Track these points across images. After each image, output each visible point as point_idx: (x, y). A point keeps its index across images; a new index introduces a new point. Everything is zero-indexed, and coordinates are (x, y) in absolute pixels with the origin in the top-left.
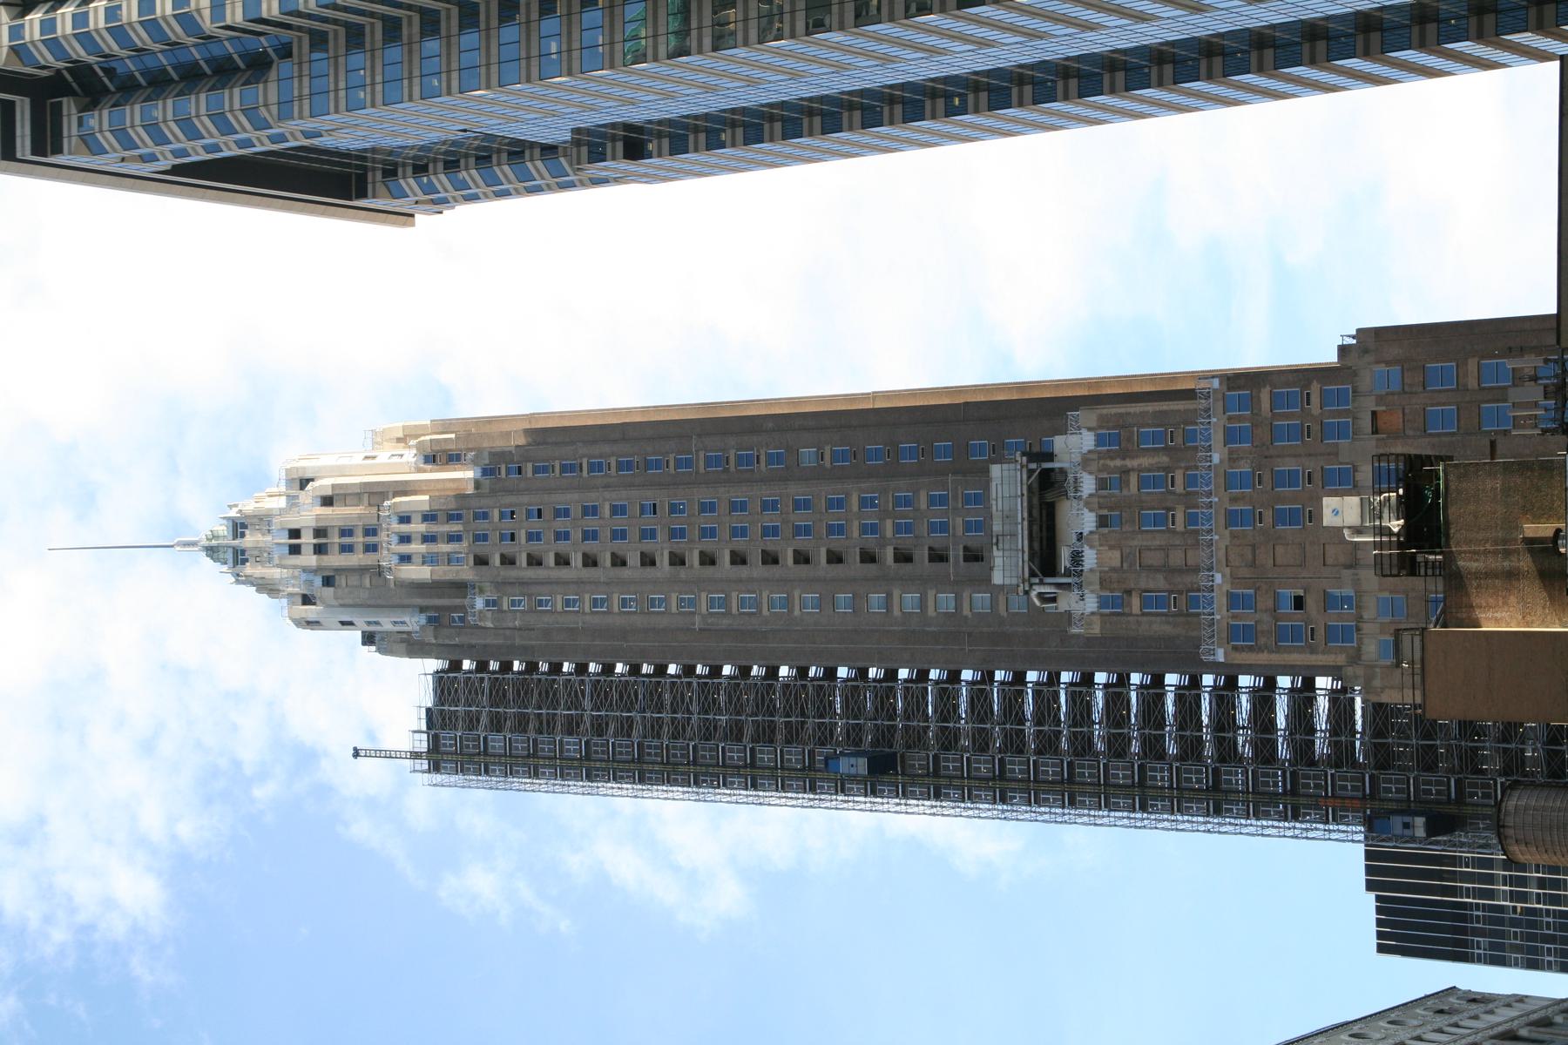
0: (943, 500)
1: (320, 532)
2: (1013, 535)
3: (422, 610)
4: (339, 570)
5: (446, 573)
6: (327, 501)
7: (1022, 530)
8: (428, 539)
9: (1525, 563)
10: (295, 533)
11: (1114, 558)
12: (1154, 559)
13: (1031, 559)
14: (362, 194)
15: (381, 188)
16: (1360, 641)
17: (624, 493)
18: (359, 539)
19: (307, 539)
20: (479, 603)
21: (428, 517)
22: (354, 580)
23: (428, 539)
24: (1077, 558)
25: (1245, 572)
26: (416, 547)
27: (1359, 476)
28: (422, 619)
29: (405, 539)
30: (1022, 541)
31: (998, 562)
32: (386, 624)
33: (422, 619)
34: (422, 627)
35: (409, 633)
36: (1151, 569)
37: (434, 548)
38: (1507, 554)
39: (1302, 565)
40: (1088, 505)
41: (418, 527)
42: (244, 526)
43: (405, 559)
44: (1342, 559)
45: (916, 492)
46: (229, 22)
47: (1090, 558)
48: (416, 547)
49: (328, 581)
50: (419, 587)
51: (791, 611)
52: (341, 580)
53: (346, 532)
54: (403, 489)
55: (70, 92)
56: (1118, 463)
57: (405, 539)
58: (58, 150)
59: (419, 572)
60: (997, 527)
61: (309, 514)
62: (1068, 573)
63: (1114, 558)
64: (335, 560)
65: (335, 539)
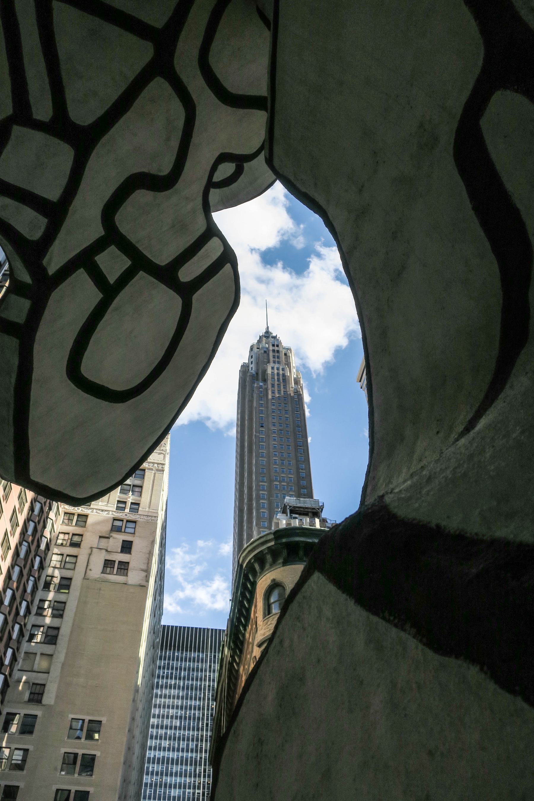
1: (278, 351)
3: (257, 374)
4: (268, 355)
5: (270, 377)
6: (285, 354)
8: (278, 374)
10: (278, 346)
19: (276, 348)
20: (261, 384)
21: (284, 375)
22: (265, 357)
23: (278, 374)
28: (254, 373)
29: (278, 369)
30: (299, 505)
33: (254, 373)
41: (281, 372)
43: (273, 368)
48: (276, 371)
49: (265, 352)
50: (265, 371)
52: (265, 355)
53: (278, 357)
57: (278, 369)
59: (269, 371)
64: (271, 354)
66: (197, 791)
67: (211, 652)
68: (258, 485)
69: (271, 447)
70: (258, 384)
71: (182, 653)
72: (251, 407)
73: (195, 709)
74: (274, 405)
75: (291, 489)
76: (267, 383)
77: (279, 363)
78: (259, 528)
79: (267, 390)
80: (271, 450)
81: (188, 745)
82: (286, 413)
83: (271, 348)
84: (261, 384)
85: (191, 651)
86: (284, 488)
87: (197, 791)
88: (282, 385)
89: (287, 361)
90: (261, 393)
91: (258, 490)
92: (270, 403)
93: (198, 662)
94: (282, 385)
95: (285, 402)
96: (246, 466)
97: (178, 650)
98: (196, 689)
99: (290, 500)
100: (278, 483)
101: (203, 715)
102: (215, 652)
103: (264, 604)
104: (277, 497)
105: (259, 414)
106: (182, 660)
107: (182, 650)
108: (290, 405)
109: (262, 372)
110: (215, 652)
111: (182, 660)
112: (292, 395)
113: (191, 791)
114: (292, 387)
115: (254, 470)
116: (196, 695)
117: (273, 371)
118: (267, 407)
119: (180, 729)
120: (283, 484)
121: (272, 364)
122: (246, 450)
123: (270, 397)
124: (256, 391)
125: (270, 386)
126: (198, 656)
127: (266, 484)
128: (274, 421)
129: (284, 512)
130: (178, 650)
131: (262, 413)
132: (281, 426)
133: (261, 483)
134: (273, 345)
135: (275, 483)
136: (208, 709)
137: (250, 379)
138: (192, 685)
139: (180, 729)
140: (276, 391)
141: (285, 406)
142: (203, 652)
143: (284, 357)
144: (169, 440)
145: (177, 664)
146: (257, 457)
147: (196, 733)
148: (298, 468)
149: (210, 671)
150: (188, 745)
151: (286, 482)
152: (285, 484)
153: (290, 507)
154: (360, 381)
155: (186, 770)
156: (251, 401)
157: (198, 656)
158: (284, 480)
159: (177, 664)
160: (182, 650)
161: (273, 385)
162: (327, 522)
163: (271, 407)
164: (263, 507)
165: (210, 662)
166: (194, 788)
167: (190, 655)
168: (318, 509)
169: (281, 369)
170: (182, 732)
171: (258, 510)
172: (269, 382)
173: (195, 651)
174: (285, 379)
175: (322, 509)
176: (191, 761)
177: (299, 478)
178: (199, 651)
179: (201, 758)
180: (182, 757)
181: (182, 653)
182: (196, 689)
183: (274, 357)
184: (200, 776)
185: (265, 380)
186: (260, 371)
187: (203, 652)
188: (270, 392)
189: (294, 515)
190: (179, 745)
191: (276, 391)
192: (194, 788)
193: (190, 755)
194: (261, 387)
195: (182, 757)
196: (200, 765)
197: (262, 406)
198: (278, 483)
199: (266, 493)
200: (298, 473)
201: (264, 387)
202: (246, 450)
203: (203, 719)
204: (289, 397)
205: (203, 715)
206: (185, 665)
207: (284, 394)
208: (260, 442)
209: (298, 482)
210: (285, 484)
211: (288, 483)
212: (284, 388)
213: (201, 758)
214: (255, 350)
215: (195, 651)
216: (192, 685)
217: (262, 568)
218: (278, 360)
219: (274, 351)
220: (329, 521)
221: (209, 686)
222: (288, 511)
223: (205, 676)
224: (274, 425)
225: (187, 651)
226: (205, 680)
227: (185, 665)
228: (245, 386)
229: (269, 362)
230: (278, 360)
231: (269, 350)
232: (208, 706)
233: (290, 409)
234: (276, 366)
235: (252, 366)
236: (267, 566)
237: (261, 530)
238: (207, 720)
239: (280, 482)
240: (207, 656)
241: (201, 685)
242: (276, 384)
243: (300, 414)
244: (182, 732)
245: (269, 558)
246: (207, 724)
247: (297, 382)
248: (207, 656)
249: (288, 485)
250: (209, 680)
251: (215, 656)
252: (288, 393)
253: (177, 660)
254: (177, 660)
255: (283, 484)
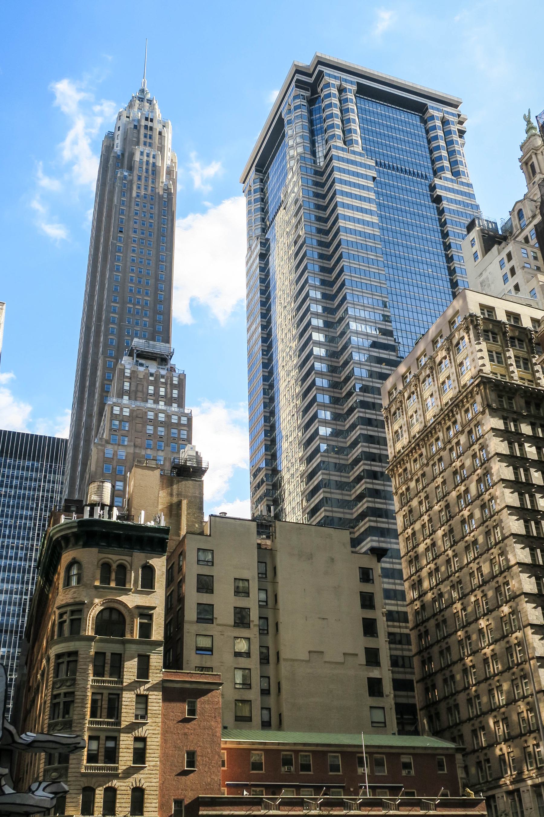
0: (145, 325)
1: (151, 128)
2: (148, 347)
3: (123, 155)
4: (139, 132)
5: (137, 165)
6: (160, 133)
7: (150, 350)
8: (148, 162)
9: (175, 500)
10: (152, 120)
11: (141, 376)
12: (140, 388)
13: (142, 351)
14: (257, 171)
15: (257, 177)
16: (112, 444)
17: (156, 228)
18: (148, 140)
19: (150, 124)
20: (126, 174)
21: (154, 165)
22: (135, 135)
23: (148, 162)
24: (142, 365)
25: (135, 414)
26: (145, 158)
27: (149, 450)
28: (119, 153)
29: (148, 156)
30: (147, 350)
31: (141, 341)
32: (118, 142)
33: (119, 153)
34: (116, 153)
35: (113, 147)
36: (137, 387)
37: (145, 164)
38: (178, 495)
39: (136, 431)
40: (157, 371)
41: (151, 160)
42: (150, 104)
43: (142, 153)
44: (136, 443)
45: (148, 318)
46: (332, 150)
47: (141, 369)
48: (145, 158)
49: (135, 127)
50: (132, 155)
51: (115, 271)
52: (135, 131)
53: (151, 137)
54: (163, 159)
55: (312, 94)
56: (169, 382)
57: (148, 156)
58: (297, 86)
59: (137, 157)
60: (151, 342)
61: (158, 127)
62: (137, 361)
63: (141, 376)
64: (142, 131)
65: (149, 133)
66: (24, 597)
67: (47, 462)
68: (108, 306)
69: (128, 259)
70: (122, 173)
71: (15, 461)
72: (111, 200)
73: (26, 519)
74: (137, 205)
75: (146, 314)
76: (132, 173)
77: (150, 145)
78: (105, 357)
79: (131, 182)
80: (129, 264)
81: (16, 554)
82: (151, 217)
83: (143, 123)
84: (126, 174)
85: (25, 459)
86: (138, 313)
87: (24, 597)
88: (150, 178)
89: (161, 144)
90: (125, 187)
91: (108, 312)
92: (133, 203)
93: (32, 471)
94: (150, 178)
95: (152, 202)
96: (98, 275)
97: (11, 457)
98: (28, 499)
99: (138, 343)
100: (131, 306)
101: (35, 525)
102: (51, 462)
103: (65, 576)
104: (129, 322)
105: (119, 214)
106: (14, 468)
107: (15, 457)
108: (157, 207)
109: (129, 156)
110: (51, 462)
111: (14, 468)
112: (161, 193)
113: (18, 596)
114: (162, 182)
115: (107, 276)
116: (28, 505)
117: (141, 157)
118: (130, 207)
119: (9, 537)
120: (137, 307)
121: (141, 148)
122: (100, 255)
123: (134, 194)
124: (118, 184)
125: (135, 178)
126: (33, 465)
127: (118, 305)
128: (136, 226)
129: (131, 355)
130: (11, 457)
131: (122, 213)
132: (143, 233)
133: (113, 304)
134: (147, 119)
135: (128, 305)
136: (40, 520)
137: (113, 161)
138: (24, 494)
139: (9, 537)
140: (143, 187)
141: (151, 208)
142: (38, 461)
143: (157, 136)
144: (4, 311)
145: (9, 472)
146: (111, 270)
147: (20, 586)
148: (156, 289)
149: (45, 482)
150: (16, 554)
151: (141, 306)
152: (140, 307)
153: (137, 351)
154: (244, 183)
155: (13, 577)
156: (112, 193)
157: (33, 465)
158: (138, 302)
159: (9, 472)
160: (15, 457)
161: (139, 178)
162: (175, 371)
163: (134, 208)
164: (112, 334)
165: (46, 472)
166: (21, 594)
167: (24, 463)
168: (168, 356)
169: (151, 156)
170: (11, 541)
171: (106, 336)
172: (136, 172)
173: (29, 460)
174: (155, 171)
175: (171, 357)
176: (19, 569)
177: (157, 301)
178: (33, 460)
179: (30, 566)
180: (10, 565)
181: (15, 461)
182: (28, 499)
183: (145, 136)
184: (27, 583)
185: (131, 169)
186: (126, 155)
187: (38, 461)
188: (135, 187)
189: (141, 361)
190: (7, 553)
191: (143, 187)
192: (21, 594)
193: (18, 563)
194: (125, 177)
195: (10, 565)
196: (29, 573)
197: (123, 204)
198: (131, 306)
199: (115, 326)
200: (156, 294)
201: (129, 178)
202: (100, 255)
203: (34, 529)
204: (157, 196)
205: (35, 525)
206: (18, 473)
207: (152, 190)
208: (116, 252)
209: (155, 305)
210: (140, 307)
211: (143, 307)
212: (153, 182)
213: (30, 566)
214: (124, 119)
215: (29, 460)
216: (24, 494)
217: (67, 546)
218: (150, 141)
219: (146, 127)
220: (177, 371)
221: (43, 496)
222: (135, 355)
223: (40, 486)
224: (135, 232)
225: (20, 458)
226: (39, 490)
227: (18, 473)
228: (107, 167)
229: (138, 144)
230: (150, 141)
231: (140, 126)
232: (40, 516)
233: (156, 212)
234: (147, 150)
235: (119, 133)
236: (71, 545)
237: (107, 359)
238: (39, 530)
239: (134, 305)
240: (42, 465)
241: (33, 495)
242: (143, 177)
243: (167, 220)
244: (11, 541)
245: (72, 540)
246: (38, 535)
247: (170, 172)
248: (42, 465)
249: (142, 309)
250: (43, 491)
251: (51, 466)
252: (157, 191)
253: (9, 468)
254: (9, 468)
255: (137, 307)
